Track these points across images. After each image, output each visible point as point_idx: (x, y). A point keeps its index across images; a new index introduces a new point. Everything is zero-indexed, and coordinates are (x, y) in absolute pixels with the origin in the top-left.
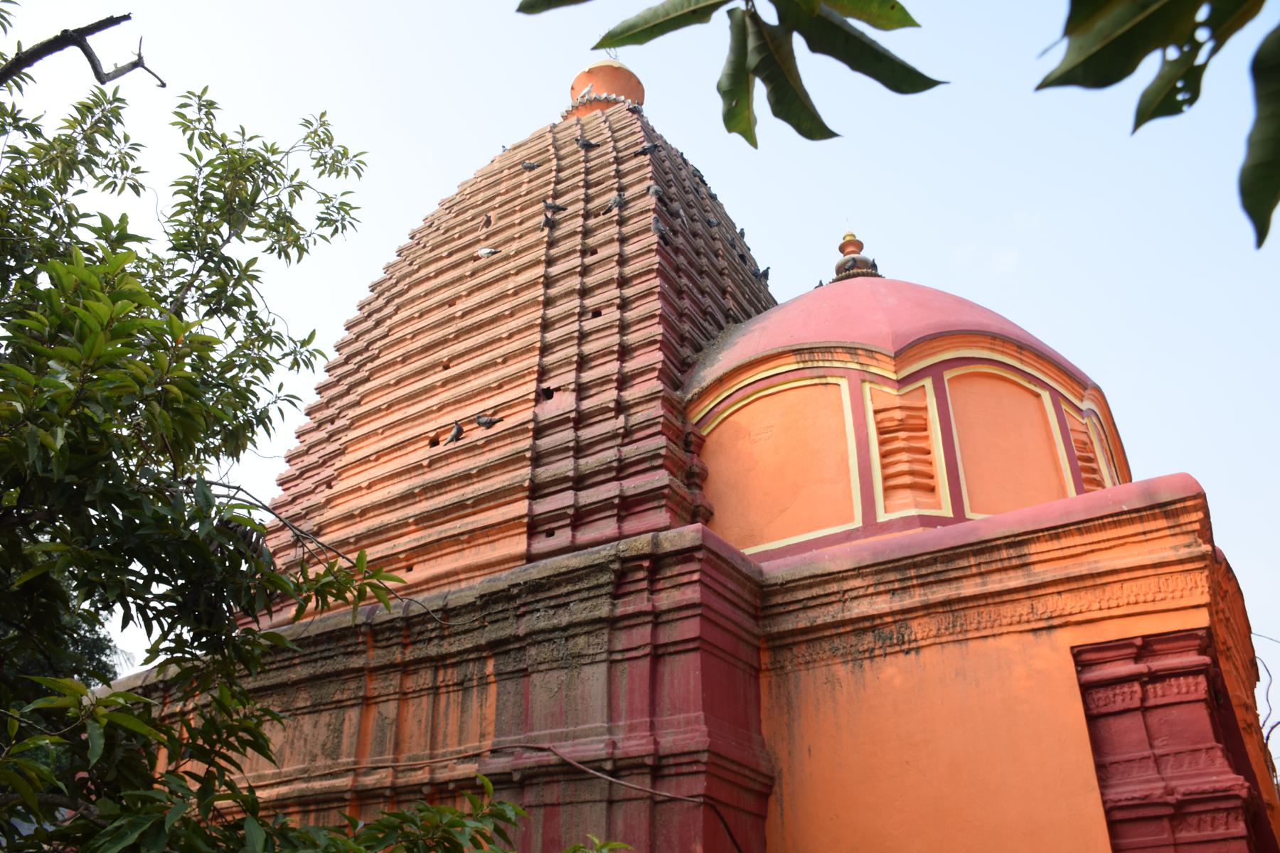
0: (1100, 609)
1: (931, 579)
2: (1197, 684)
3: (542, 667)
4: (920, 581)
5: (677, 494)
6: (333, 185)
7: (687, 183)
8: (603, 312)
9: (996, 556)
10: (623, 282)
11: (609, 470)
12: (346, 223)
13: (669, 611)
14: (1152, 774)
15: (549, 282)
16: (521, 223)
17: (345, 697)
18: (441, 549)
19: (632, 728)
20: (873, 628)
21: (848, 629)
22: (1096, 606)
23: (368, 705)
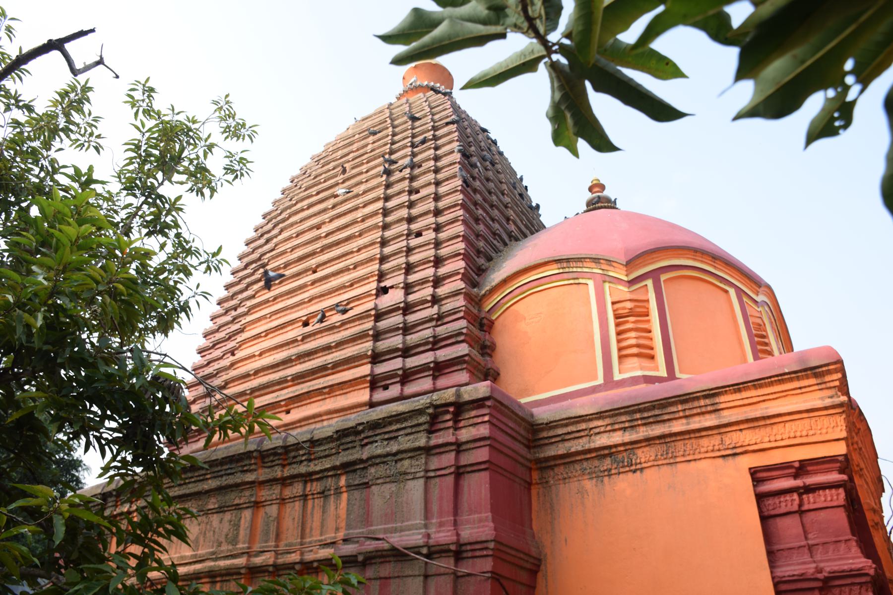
1: (651, 420)
2: (838, 495)
3: (379, 481)
4: (643, 422)
5: (474, 360)
6: (235, 146)
7: (483, 144)
8: (424, 233)
10: (437, 213)
14: (807, 558)
15: (386, 212)
16: (367, 172)
17: (242, 501)
18: (310, 398)
19: (441, 524)
21: (593, 455)
22: (767, 439)
23: (258, 507)
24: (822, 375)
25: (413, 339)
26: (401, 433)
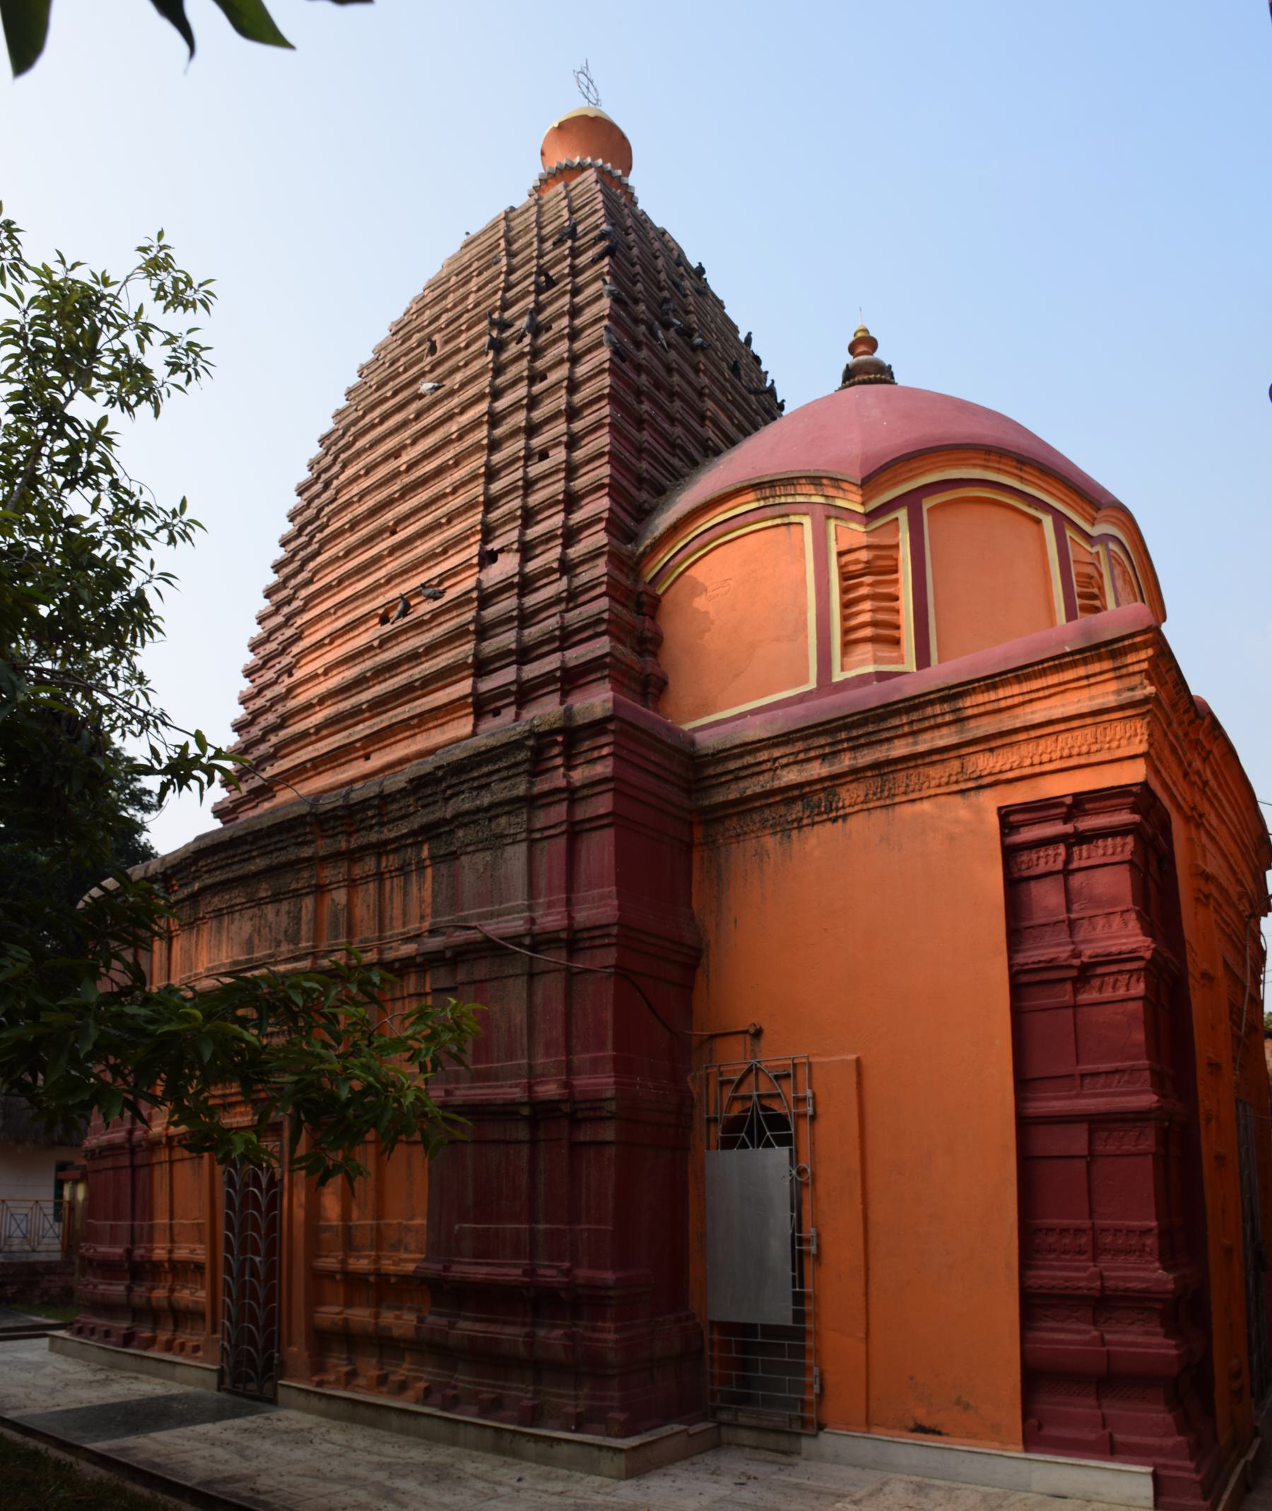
0: (1032, 765)
1: (862, 741)
2: (1123, 845)
3: (470, 849)
4: (851, 744)
5: (622, 663)
6: (176, 321)
7: (663, 276)
8: (551, 453)
9: (929, 711)
10: (572, 413)
11: (551, 639)
12: (199, 368)
13: (584, 786)
14: (1064, 937)
15: (494, 419)
16: (467, 347)
17: (300, 886)
18: (395, 735)
19: (550, 905)
20: (802, 797)
21: (778, 798)
22: (1028, 762)
23: (323, 893)
24: (1124, 652)
25: (532, 633)
26: (495, 778)
